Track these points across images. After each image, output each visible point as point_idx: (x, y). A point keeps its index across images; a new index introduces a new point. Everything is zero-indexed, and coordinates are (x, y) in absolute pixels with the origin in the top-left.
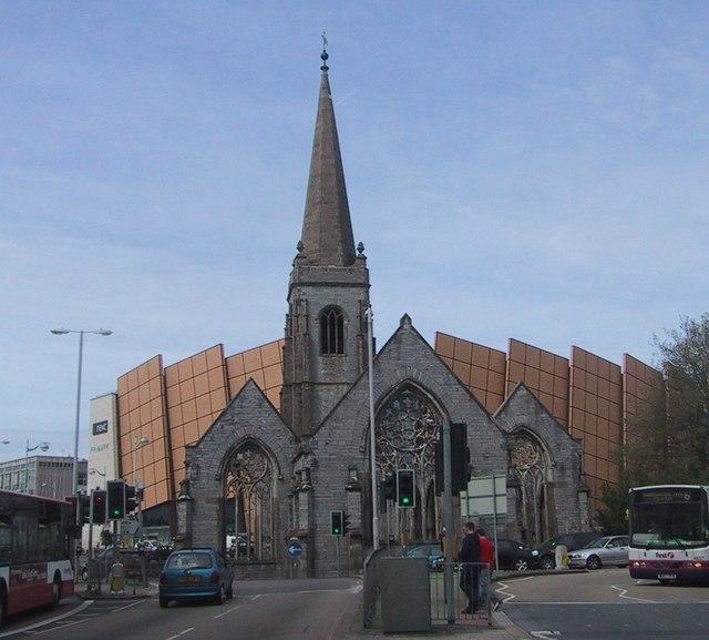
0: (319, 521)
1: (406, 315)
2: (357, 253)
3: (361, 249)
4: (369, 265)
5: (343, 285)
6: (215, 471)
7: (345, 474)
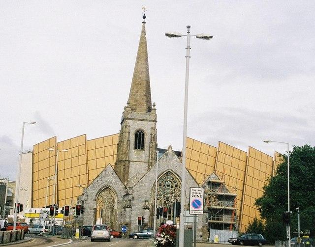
0: (132, 219)
1: (170, 146)
2: (152, 107)
3: (154, 105)
4: (157, 112)
5: (146, 120)
6: (94, 197)
7: (144, 203)
